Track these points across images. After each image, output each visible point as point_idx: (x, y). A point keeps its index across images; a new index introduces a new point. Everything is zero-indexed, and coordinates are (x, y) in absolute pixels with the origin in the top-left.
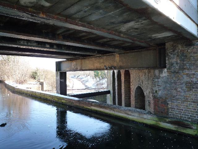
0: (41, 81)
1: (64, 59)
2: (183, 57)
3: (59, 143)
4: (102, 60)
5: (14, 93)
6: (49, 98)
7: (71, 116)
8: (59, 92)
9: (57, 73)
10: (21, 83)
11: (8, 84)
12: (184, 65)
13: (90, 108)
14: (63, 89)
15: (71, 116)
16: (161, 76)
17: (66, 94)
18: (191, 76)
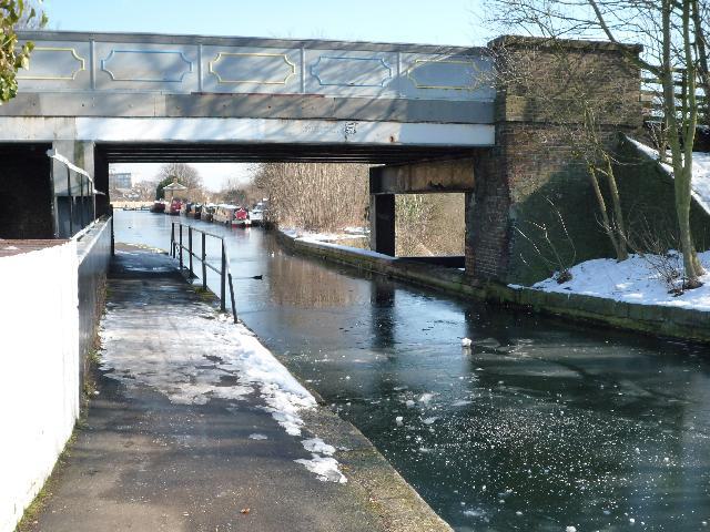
10: (311, 226)
14: (384, 236)
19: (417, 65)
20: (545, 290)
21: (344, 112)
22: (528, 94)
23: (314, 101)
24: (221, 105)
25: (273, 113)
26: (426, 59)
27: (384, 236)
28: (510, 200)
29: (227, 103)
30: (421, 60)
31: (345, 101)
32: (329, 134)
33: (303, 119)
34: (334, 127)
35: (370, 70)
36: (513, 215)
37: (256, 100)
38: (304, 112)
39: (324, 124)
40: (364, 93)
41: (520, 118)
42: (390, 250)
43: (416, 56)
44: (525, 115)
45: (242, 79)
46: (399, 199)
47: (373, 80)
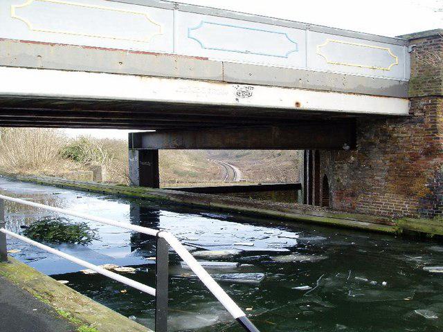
42: (155, 184)
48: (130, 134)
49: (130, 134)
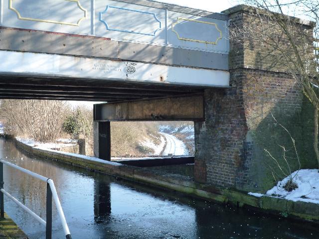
0: (81, 136)
1: (105, 101)
2: (218, 108)
3: (91, 231)
4: (151, 106)
5: (31, 157)
6: (83, 164)
7: (119, 195)
8: (98, 154)
9: (96, 124)
10: (43, 139)
11: (21, 141)
12: (219, 117)
13: (132, 176)
14: (104, 149)
15: (119, 195)
16: (201, 130)
17: (109, 160)
18: (225, 132)
19: (179, 22)
20: (286, 198)
21: (126, 54)
22: (256, 50)
23: (102, 43)
24: (20, 39)
25: (68, 50)
26: (186, 17)
27: (104, 149)
28: (246, 129)
29: (25, 38)
30: (181, 18)
31: (126, 45)
32: (114, 72)
33: (93, 57)
34: (119, 66)
35: (146, 22)
36: (249, 139)
37: (53, 38)
38: (94, 51)
39: (110, 63)
40: (140, 40)
41: (252, 67)
42: (108, 157)
43: (178, 14)
44: (256, 65)
45: (40, 19)
46: (112, 123)
47: (147, 30)
48: (94, 105)
49: (94, 105)
